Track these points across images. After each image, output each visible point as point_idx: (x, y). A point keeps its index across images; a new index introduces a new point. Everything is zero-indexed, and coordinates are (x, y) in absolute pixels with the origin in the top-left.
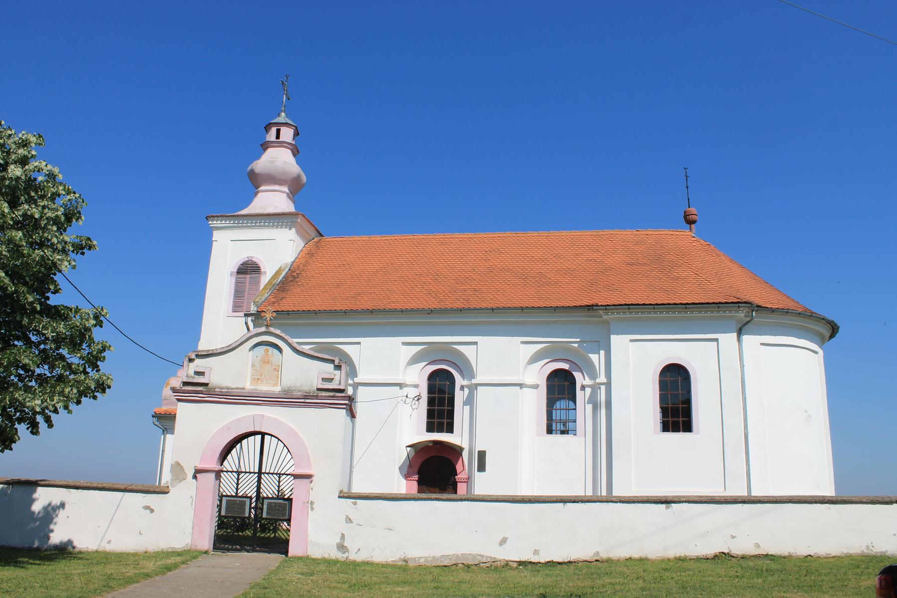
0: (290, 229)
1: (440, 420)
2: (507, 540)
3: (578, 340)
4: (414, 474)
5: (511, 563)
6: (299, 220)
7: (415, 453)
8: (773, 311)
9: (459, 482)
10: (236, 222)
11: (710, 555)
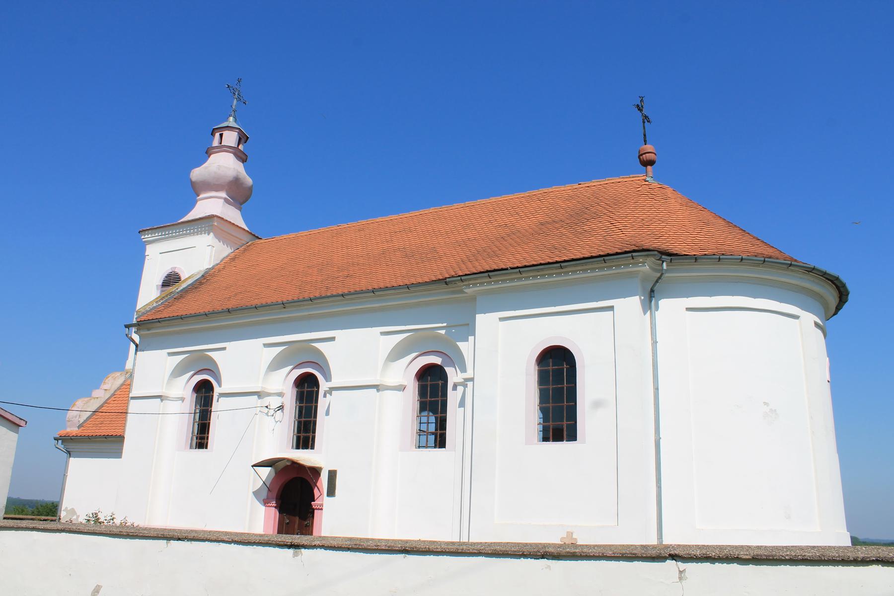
0: (208, 235)
1: (305, 435)
3: (445, 324)
6: (216, 224)
7: (276, 474)
8: (696, 258)
9: (316, 509)
10: (163, 234)
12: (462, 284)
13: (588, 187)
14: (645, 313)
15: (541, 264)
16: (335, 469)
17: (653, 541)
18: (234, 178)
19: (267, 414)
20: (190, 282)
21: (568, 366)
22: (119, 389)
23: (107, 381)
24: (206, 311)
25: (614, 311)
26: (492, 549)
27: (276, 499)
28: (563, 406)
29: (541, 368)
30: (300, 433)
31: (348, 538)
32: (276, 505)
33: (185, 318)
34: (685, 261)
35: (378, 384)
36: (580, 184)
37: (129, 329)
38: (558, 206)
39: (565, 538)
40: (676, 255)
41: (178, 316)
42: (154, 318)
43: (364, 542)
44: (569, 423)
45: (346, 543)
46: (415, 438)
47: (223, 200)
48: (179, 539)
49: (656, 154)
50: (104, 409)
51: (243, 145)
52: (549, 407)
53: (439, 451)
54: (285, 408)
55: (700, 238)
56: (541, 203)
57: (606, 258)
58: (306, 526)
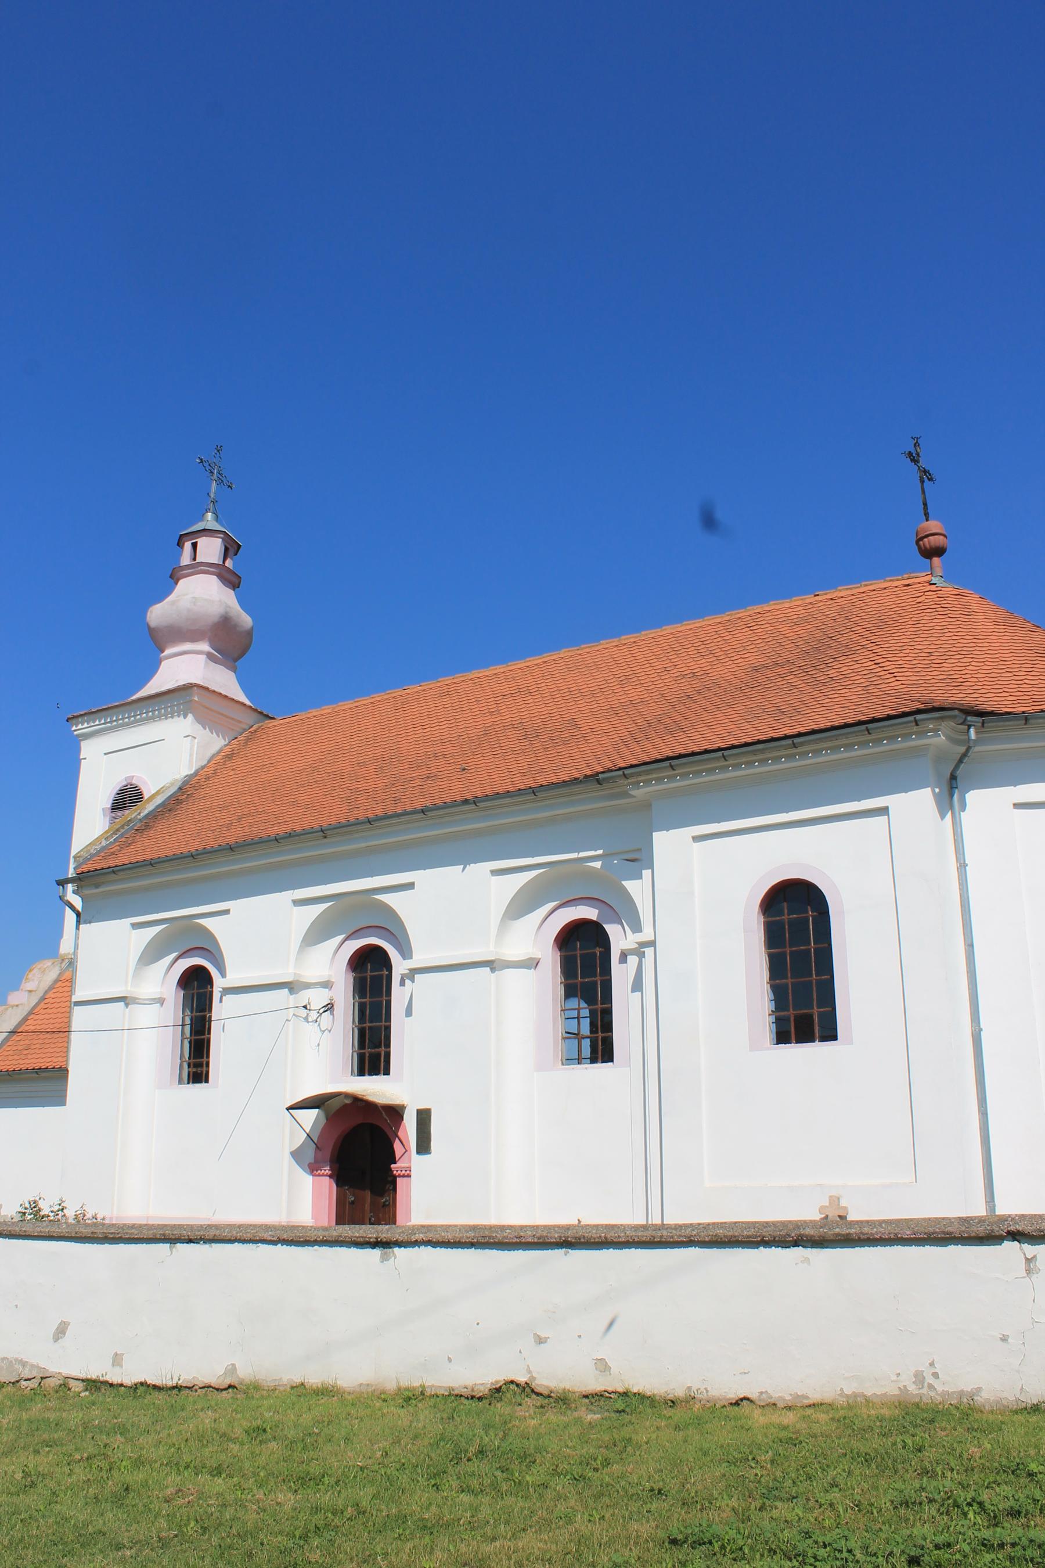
0: (185, 717)
2: (67, 1328)
3: (600, 852)
4: (327, 1166)
5: (72, 1383)
6: (196, 699)
7: (327, 1120)
8: (1026, 718)
9: (400, 1176)
10: (109, 720)
11: (482, 1388)
12: (626, 782)
13: (831, 599)
14: (943, 816)
15: (759, 742)
16: (428, 1107)
17: (979, 1210)
18: (221, 617)
19: (306, 1019)
20: (159, 800)
21: (815, 914)
22: (51, 988)
23: (30, 976)
24: (193, 850)
25: (888, 815)
26: (711, 1233)
27: (330, 1161)
28: (811, 982)
29: (770, 919)
30: (364, 1049)
31: (469, 1226)
32: (330, 1172)
33: (156, 863)
34: (1007, 723)
35: (493, 958)
36: (818, 595)
37: (63, 887)
38: (782, 637)
39: (826, 1206)
40: (992, 713)
41: (144, 860)
42: (104, 866)
43: (497, 1232)
44: (822, 1010)
45: (468, 1235)
46: (560, 1048)
47: (205, 656)
48: (190, 1241)
49: (945, 536)
50: (29, 1026)
51: (232, 559)
52: (787, 985)
53: (601, 1069)
54: (335, 1007)
55: (1032, 682)
56: (752, 632)
57: (870, 726)
58: (384, 1205)
